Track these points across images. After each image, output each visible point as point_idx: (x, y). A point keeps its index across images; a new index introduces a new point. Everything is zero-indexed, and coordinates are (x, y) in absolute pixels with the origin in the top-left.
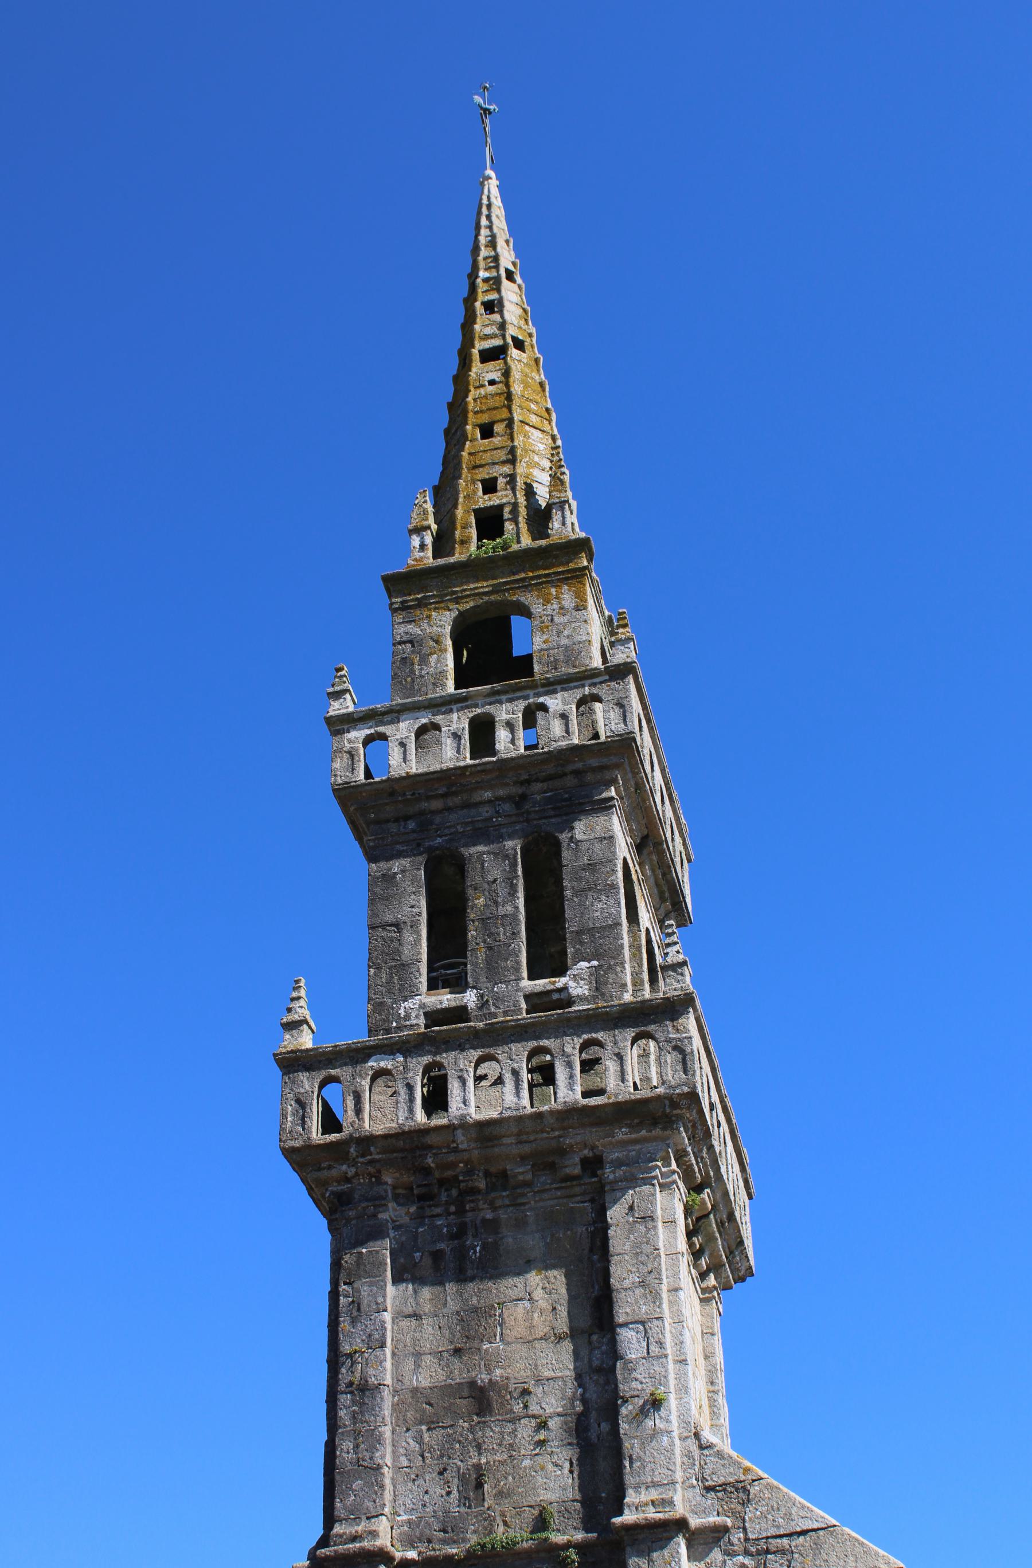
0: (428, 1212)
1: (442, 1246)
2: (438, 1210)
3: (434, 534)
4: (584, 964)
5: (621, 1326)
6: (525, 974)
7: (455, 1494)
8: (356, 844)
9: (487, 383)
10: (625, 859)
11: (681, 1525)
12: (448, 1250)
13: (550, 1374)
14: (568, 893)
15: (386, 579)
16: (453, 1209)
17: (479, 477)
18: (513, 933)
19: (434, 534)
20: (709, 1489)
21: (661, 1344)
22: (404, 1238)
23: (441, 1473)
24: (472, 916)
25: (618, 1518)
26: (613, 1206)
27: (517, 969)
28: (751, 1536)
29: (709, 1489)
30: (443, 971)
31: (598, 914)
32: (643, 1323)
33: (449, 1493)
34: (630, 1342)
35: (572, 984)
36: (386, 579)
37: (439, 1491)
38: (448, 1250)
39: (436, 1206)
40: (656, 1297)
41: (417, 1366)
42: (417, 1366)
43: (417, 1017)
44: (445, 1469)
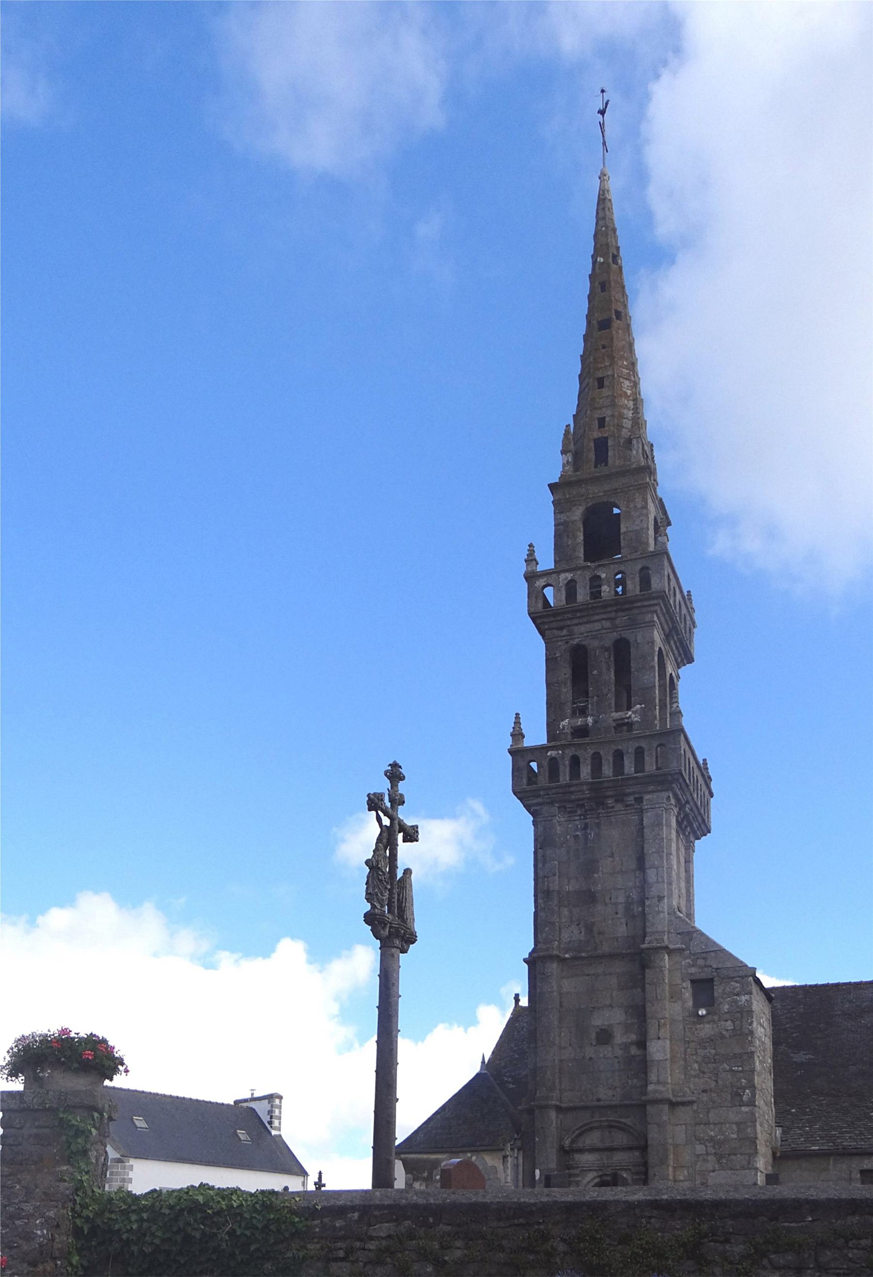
0: (573, 818)
1: (578, 833)
2: (576, 818)
3: (666, 563)
4: (638, 706)
5: (648, 869)
6: (613, 710)
7: (583, 933)
8: (540, 637)
9: (601, 347)
10: (660, 648)
11: (666, 948)
12: (580, 835)
13: (619, 887)
14: (633, 670)
15: (549, 485)
16: (582, 817)
17: (597, 416)
18: (609, 690)
19: (666, 563)
20: (678, 934)
21: (663, 877)
22: (563, 829)
23: (578, 925)
24: (600, 435)
25: (625, 769)
26: (706, 1200)
27: (610, 707)
28: (692, 952)
29: (678, 934)
30: (579, 704)
31: (646, 681)
32: (657, 868)
33: (581, 933)
34: (651, 875)
35: (633, 716)
36: (549, 485)
37: (576, 932)
38: (580, 835)
39: (576, 816)
40: (662, 857)
41: (569, 882)
42: (569, 882)
43: (567, 729)
44: (579, 924)
